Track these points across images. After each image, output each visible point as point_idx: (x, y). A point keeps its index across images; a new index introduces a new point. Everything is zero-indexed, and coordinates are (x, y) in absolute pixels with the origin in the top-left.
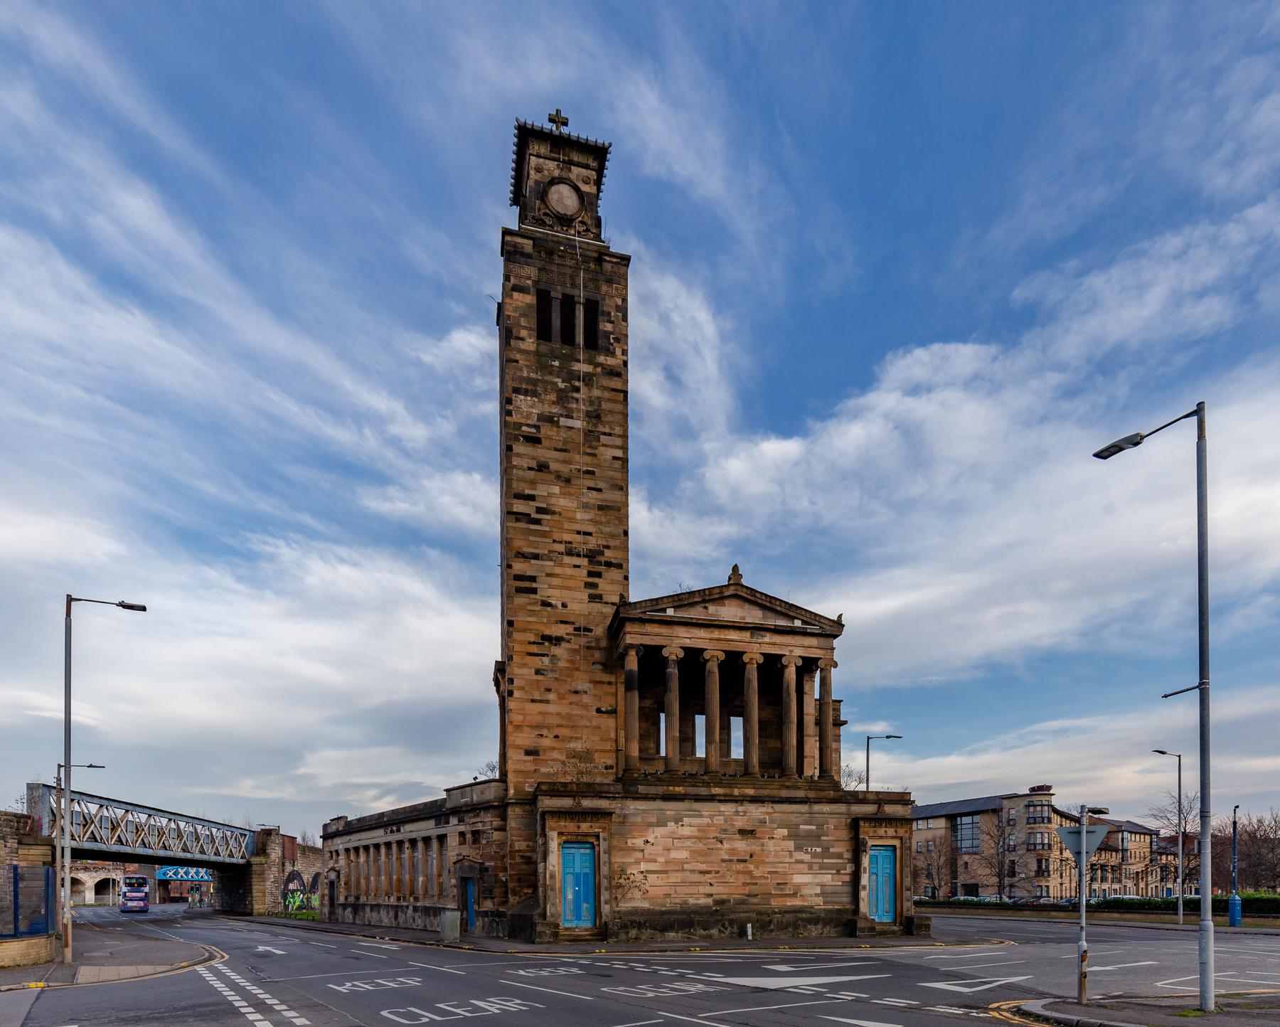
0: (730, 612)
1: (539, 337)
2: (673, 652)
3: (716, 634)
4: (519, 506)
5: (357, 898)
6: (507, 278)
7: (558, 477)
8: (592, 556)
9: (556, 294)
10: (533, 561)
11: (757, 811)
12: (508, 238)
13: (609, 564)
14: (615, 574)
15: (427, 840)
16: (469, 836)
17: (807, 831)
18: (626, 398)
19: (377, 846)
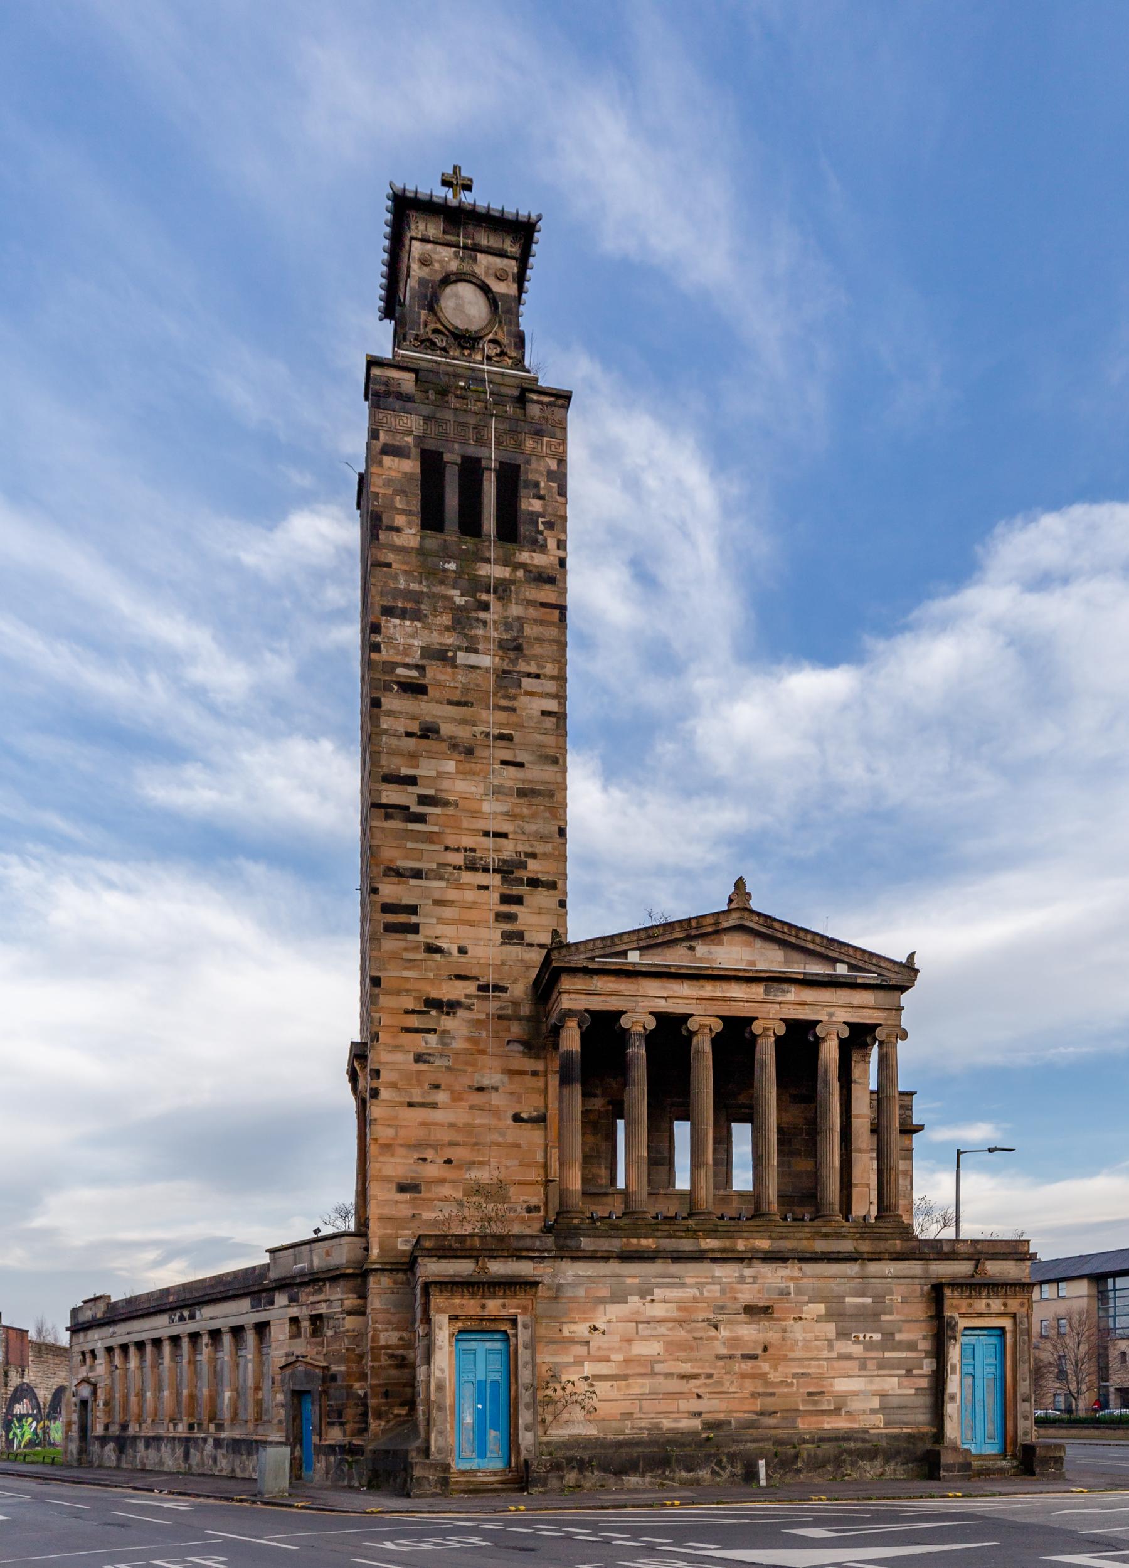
0: (731, 954)
2: (638, 1020)
3: (709, 989)
4: (392, 795)
7: (454, 746)
8: (507, 870)
9: (452, 457)
10: (412, 882)
11: (775, 1276)
12: (376, 371)
13: (534, 883)
14: (544, 898)
15: (237, 1331)
16: (305, 1325)
17: (857, 1306)
18: (563, 618)
19: (157, 1342)
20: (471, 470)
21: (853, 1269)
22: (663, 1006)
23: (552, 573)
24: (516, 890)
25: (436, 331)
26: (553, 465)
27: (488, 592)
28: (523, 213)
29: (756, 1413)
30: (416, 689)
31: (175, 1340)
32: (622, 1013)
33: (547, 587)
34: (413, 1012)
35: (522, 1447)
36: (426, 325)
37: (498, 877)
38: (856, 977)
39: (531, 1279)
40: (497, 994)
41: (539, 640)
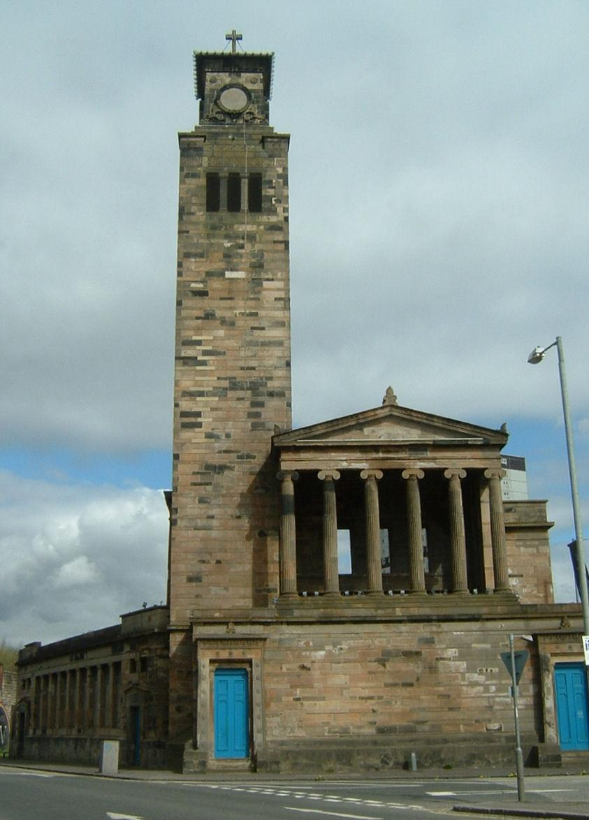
1: (208, 210)
4: (188, 352)
5: (44, 732)
6: (182, 169)
7: (223, 322)
8: (254, 387)
10: (198, 399)
12: (182, 140)
13: (271, 394)
14: (274, 403)
15: (105, 667)
16: (139, 665)
17: (482, 651)
18: (287, 247)
19: (64, 674)
20: (234, 180)
21: (475, 626)
22: (345, 465)
23: (280, 225)
24: (260, 399)
25: (217, 113)
26: (280, 170)
27: (243, 238)
28: (264, 53)
29: (413, 722)
30: (202, 294)
31: (73, 672)
32: (318, 471)
33: (277, 232)
34: (198, 473)
35: (256, 744)
36: (212, 111)
37: (249, 392)
38: (468, 440)
39: (263, 637)
40: (249, 460)
41: (274, 261)
